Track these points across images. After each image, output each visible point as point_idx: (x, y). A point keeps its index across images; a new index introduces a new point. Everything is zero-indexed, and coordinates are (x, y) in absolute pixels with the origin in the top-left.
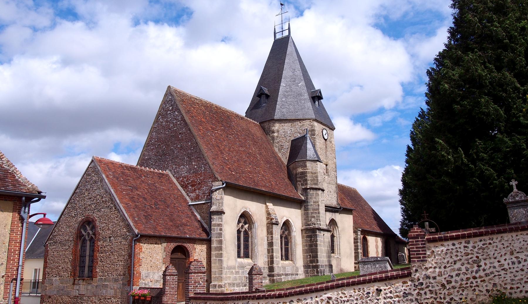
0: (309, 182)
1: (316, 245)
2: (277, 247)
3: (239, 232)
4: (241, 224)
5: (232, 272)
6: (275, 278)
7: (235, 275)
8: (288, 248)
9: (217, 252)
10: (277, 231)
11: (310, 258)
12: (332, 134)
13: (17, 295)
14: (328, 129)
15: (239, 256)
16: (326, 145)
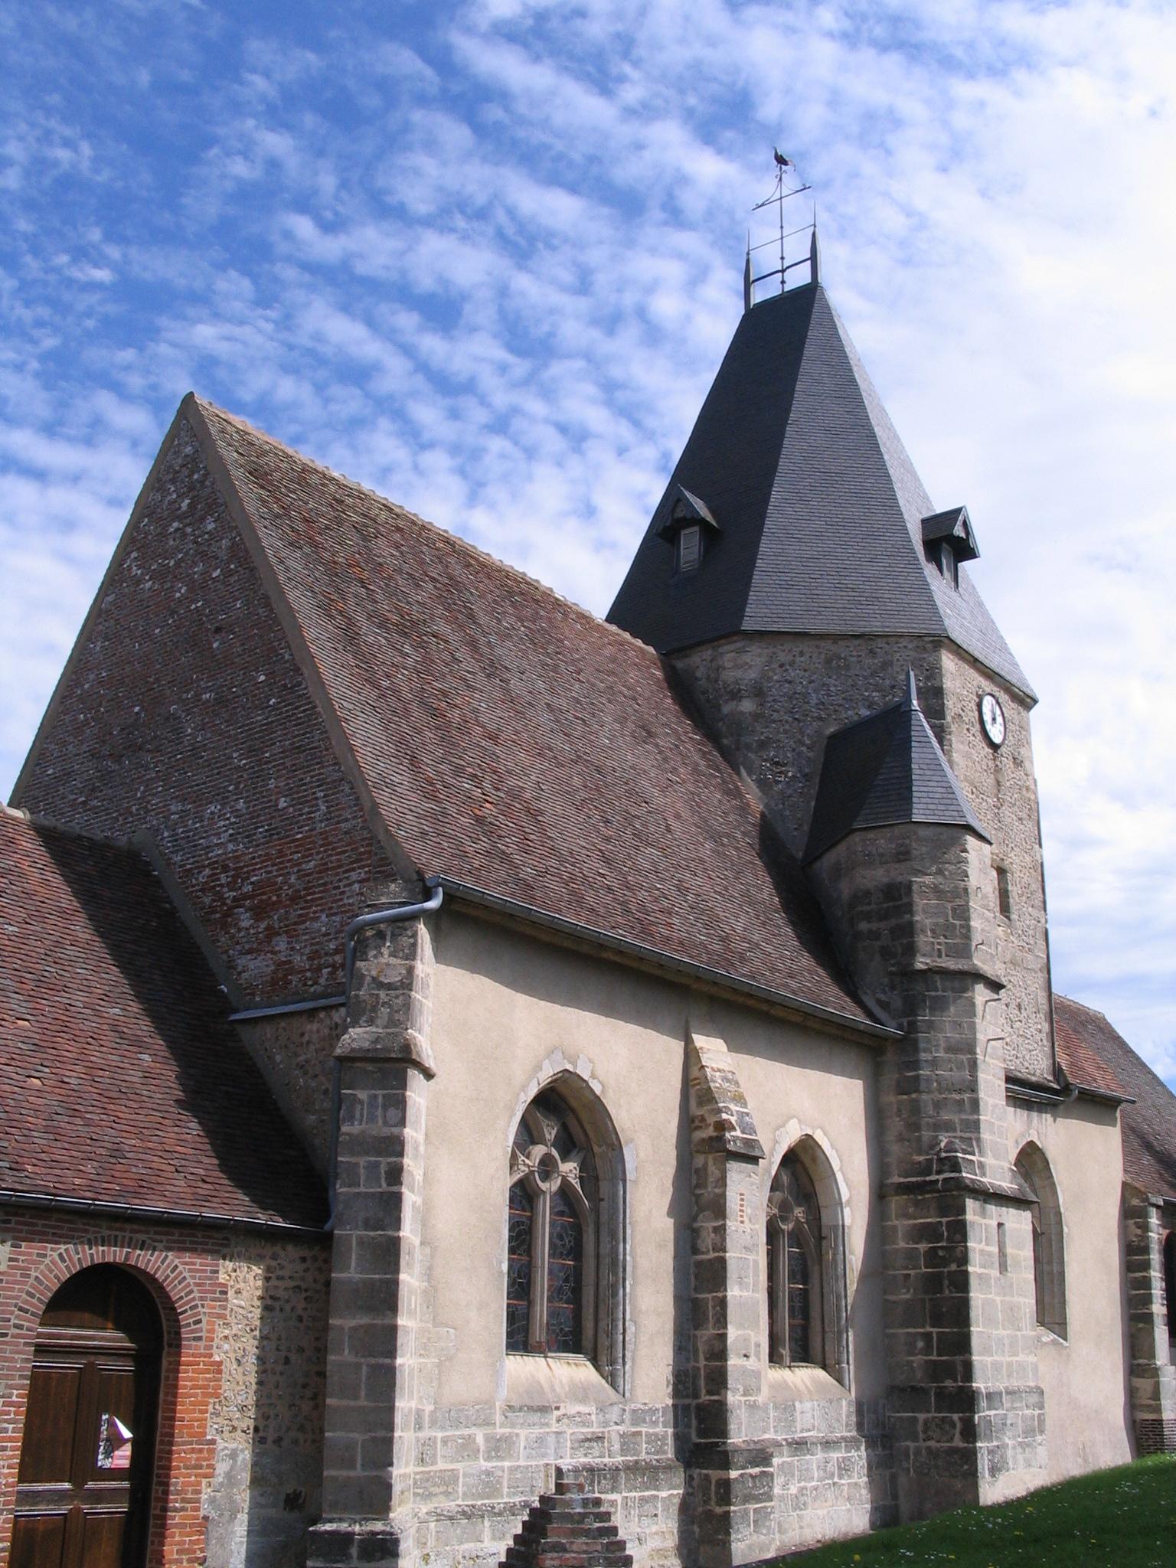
0: (923, 940)
1: (961, 1282)
2: (747, 1292)
3: (523, 1195)
4: (538, 1151)
5: (470, 1439)
6: (734, 1474)
7: (485, 1465)
8: (805, 1294)
9: (364, 1320)
10: (748, 1199)
11: (928, 1349)
12: (1024, 728)
13: (227, 1311)
14: (1004, 697)
15: (520, 1340)
16: (998, 770)
